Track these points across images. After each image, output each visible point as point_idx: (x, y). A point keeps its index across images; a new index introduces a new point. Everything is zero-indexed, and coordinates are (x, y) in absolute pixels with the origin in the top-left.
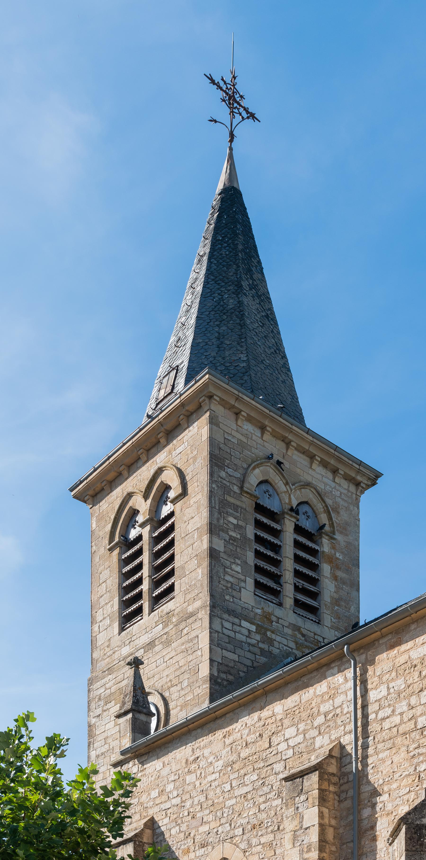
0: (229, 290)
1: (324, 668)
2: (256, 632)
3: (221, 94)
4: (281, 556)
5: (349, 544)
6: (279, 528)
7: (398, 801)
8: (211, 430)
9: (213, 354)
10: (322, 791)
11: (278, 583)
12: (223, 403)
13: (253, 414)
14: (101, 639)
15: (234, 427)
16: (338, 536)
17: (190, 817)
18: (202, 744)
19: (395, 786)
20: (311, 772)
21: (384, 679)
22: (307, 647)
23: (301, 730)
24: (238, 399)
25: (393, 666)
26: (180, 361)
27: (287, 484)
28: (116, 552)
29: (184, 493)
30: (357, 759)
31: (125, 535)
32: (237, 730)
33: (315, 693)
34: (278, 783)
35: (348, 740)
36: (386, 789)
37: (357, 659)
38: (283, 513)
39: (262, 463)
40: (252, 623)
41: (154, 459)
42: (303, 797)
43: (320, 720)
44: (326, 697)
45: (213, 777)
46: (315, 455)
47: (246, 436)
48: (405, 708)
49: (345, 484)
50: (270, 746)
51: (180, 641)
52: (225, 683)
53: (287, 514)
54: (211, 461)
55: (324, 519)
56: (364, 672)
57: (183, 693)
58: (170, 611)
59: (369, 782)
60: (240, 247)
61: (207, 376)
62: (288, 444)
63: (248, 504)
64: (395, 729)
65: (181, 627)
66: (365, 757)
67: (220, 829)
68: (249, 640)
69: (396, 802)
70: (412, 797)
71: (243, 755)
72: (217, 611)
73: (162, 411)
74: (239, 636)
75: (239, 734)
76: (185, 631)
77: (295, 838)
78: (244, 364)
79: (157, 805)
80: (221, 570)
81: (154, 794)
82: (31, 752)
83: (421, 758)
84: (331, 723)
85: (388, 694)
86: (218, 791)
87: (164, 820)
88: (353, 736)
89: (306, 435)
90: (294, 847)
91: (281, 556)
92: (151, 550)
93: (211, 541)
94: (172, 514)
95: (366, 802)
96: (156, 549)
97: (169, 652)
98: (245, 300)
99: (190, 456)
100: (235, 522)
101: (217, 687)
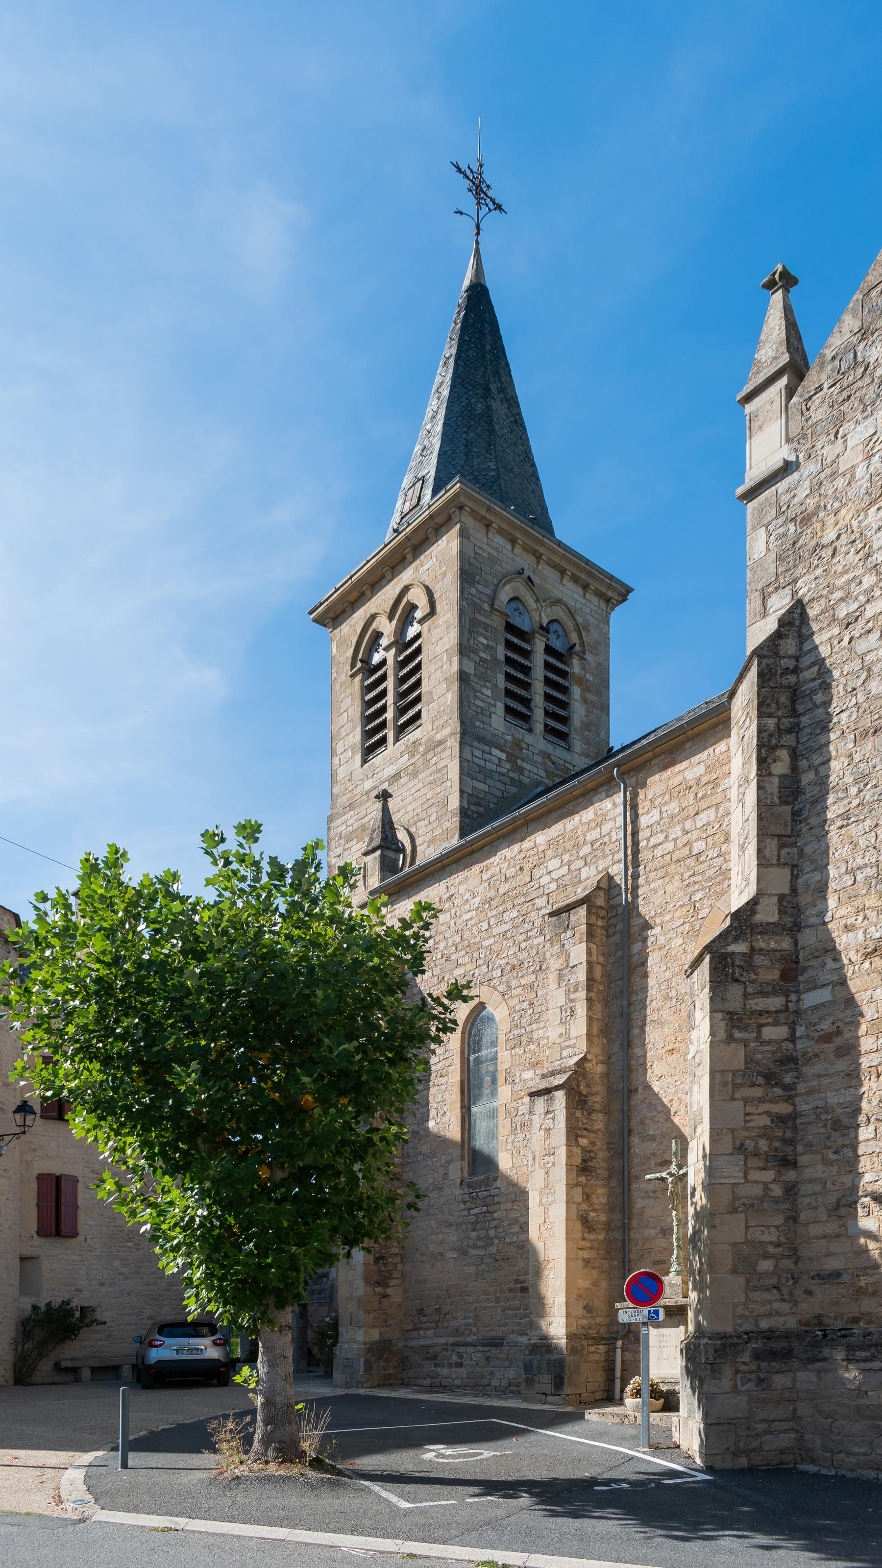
0: (476, 394)
1: (591, 794)
2: (506, 761)
3: (467, 184)
4: (531, 679)
5: (599, 664)
6: (529, 649)
7: (671, 934)
8: (461, 543)
9: (461, 462)
10: (589, 925)
11: (528, 707)
12: (474, 514)
13: (504, 526)
14: (342, 773)
15: (485, 540)
16: (588, 656)
17: (444, 959)
18: (457, 880)
19: (667, 917)
20: (579, 906)
21: (657, 803)
22: (557, 775)
23: (565, 861)
24: (489, 509)
25: (667, 788)
26: (427, 471)
27: (537, 601)
28: (359, 678)
29: (432, 612)
30: (627, 890)
31: (366, 661)
32: (495, 864)
33: (580, 820)
34: (541, 919)
35: (617, 870)
36: (658, 921)
37: (627, 782)
38: (534, 632)
39: (512, 579)
40: (502, 751)
41: (400, 577)
42: (569, 933)
43: (586, 849)
44: (593, 825)
45: (469, 915)
46: (566, 570)
47: (496, 549)
48: (679, 833)
49: (595, 600)
50: (531, 881)
51: (427, 772)
52: (475, 815)
53: (538, 633)
54: (461, 576)
55: (574, 638)
56: (635, 795)
57: (430, 827)
59: (639, 915)
60: (488, 348)
61: (458, 485)
62: (539, 557)
63: (498, 622)
64: (669, 856)
65: (429, 756)
66: (636, 888)
67: (477, 972)
68: (499, 769)
69: (669, 936)
70: (687, 929)
71: (501, 891)
72: (468, 739)
73: (409, 525)
74: (490, 766)
75: (498, 869)
76: (433, 761)
77: (560, 977)
78: (494, 473)
80: (472, 694)
82: (320, 884)
83: (697, 887)
84: (598, 853)
85: (661, 819)
86: (474, 930)
88: (622, 865)
89: (557, 548)
90: (559, 987)
91: (531, 679)
92: (396, 675)
93: (461, 663)
94: (418, 636)
95: (636, 936)
96: (401, 674)
97: (416, 784)
98: (494, 405)
99: (440, 572)
100: (485, 642)
101: (467, 820)
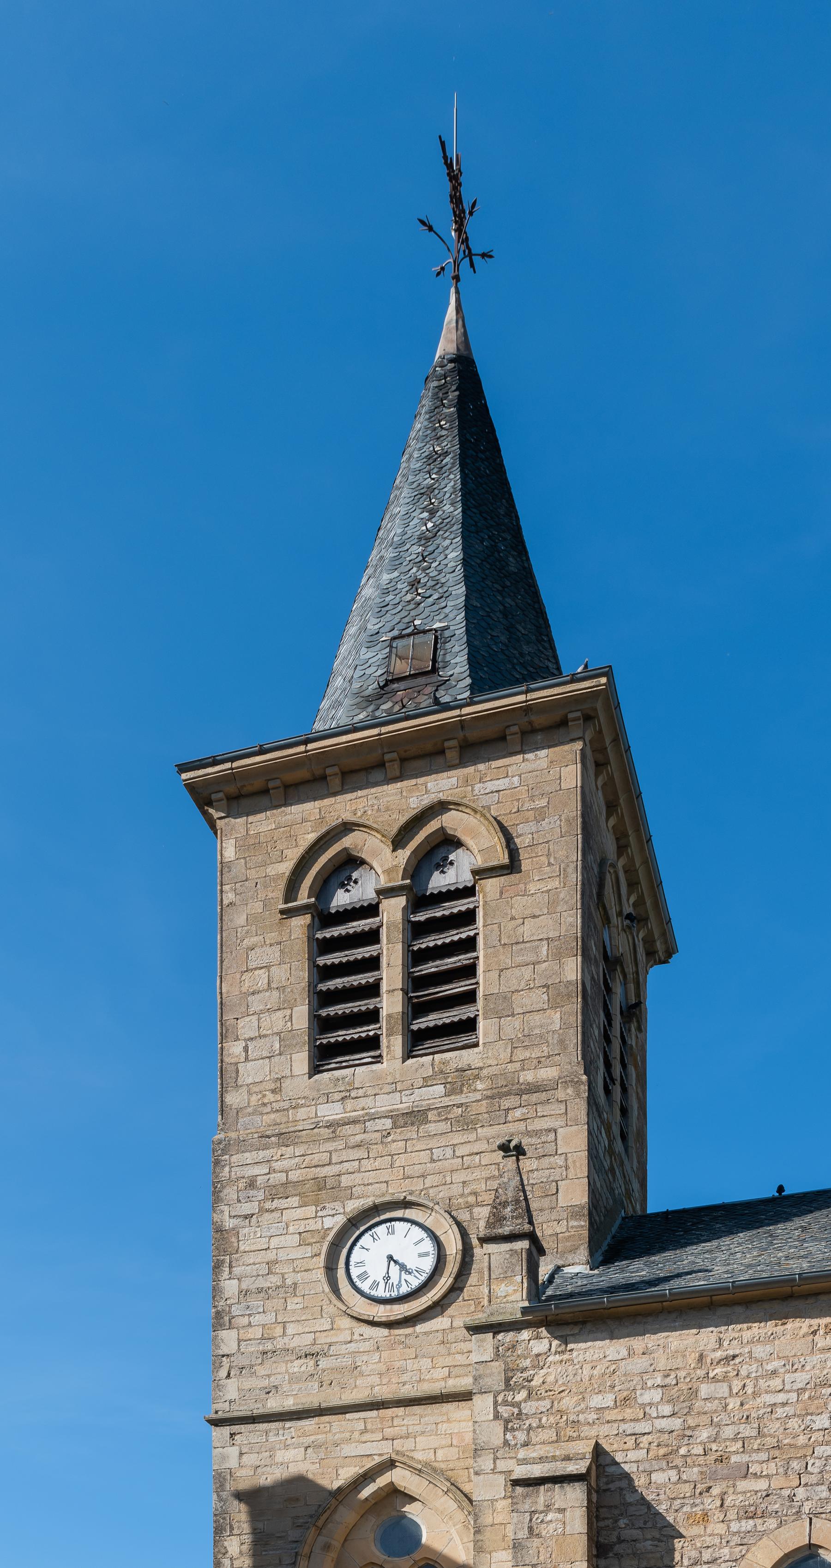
45: (781, 1398)
79: (608, 1422)
81: (608, 1400)
87: (629, 1453)
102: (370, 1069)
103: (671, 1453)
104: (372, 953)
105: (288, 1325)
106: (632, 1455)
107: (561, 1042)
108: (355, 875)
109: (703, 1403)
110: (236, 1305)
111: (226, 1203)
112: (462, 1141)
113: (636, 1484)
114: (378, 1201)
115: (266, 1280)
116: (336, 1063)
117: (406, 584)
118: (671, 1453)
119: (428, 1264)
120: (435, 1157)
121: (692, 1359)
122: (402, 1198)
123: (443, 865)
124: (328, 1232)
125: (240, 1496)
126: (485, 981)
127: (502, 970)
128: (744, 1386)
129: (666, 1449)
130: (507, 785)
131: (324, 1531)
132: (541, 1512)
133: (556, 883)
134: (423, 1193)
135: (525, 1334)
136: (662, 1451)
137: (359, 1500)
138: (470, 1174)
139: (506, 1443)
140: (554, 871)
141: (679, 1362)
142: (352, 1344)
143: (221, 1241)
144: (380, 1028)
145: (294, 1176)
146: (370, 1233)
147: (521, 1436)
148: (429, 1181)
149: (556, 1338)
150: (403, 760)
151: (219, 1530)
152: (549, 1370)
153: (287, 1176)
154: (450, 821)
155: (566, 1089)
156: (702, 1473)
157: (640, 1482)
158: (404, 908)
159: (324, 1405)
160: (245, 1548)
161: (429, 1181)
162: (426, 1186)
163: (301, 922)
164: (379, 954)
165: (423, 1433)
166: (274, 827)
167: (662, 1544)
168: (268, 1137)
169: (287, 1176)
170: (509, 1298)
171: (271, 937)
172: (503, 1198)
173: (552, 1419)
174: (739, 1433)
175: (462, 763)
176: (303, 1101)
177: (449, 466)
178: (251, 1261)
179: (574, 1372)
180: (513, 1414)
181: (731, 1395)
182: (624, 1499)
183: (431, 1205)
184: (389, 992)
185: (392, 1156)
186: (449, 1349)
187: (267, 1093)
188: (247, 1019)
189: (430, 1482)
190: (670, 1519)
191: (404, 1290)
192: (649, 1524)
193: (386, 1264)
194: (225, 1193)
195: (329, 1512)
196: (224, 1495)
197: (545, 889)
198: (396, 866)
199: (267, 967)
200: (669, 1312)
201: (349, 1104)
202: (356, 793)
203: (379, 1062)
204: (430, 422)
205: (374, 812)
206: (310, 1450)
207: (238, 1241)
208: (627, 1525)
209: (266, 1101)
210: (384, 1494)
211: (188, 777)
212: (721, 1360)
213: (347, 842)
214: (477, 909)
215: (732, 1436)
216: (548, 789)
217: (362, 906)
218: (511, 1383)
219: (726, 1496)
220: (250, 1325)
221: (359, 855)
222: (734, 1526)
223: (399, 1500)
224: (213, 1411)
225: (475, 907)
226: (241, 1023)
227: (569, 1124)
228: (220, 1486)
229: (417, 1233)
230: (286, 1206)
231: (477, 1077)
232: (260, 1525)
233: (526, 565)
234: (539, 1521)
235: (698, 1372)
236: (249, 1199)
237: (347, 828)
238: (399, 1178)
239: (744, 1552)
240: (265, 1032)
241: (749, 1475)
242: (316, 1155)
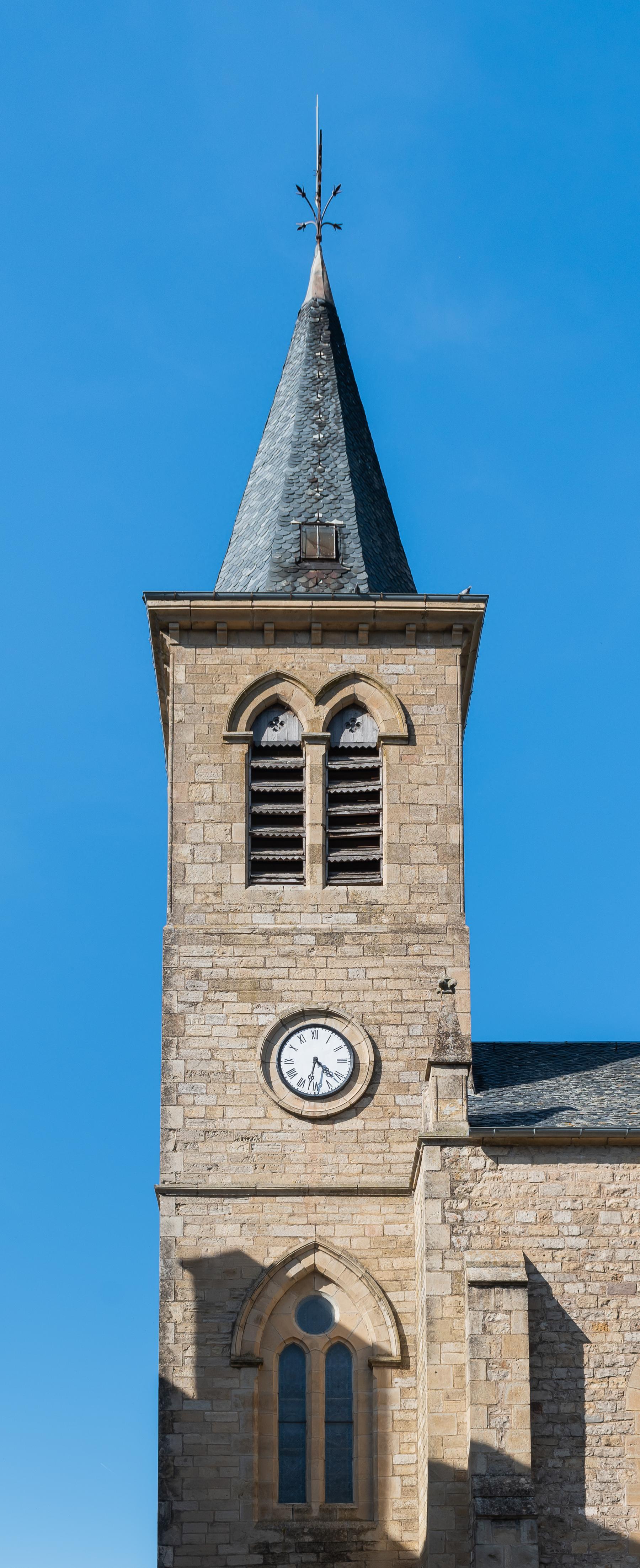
58: (374, 902)
79: (531, 1236)
81: (529, 1216)
102: (296, 889)
103: (578, 1268)
104: (297, 788)
105: (227, 1108)
106: (550, 1267)
107: (448, 894)
108: (281, 718)
109: (602, 1227)
110: (183, 1084)
111: (174, 988)
112: (372, 966)
113: (554, 1292)
114: (306, 1007)
115: (209, 1065)
116: (267, 878)
117: (306, 480)
118: (578, 1268)
119: (345, 1070)
120: (350, 976)
121: (593, 1189)
122: (326, 1008)
123: (352, 725)
124: (262, 1028)
125: (185, 1264)
126: (388, 831)
127: (401, 824)
128: (632, 1216)
129: (575, 1264)
130: (404, 671)
131: (257, 1305)
132: (492, 1312)
133: (441, 760)
134: (341, 1006)
135: (466, 1151)
136: (572, 1266)
137: (288, 1277)
138: (378, 996)
139: (452, 1245)
140: (441, 750)
141: (583, 1190)
142: (282, 1133)
143: (170, 1023)
144: (303, 855)
145: (234, 973)
146: (298, 1034)
147: (464, 1241)
148: (346, 996)
149: (490, 1157)
150: (324, 631)
151: (164, 1295)
152: (485, 1185)
153: (228, 972)
154: (360, 689)
155: (453, 935)
156: (602, 1288)
157: (556, 1291)
158: (324, 756)
159: (259, 1187)
160: (189, 1314)
161: (346, 996)
162: (343, 1000)
163: (241, 749)
164: (302, 790)
165: (341, 1221)
166: (217, 662)
167: (574, 1347)
168: (212, 934)
169: (228, 972)
170: (452, 1117)
171: (215, 757)
172: (445, 1029)
173: (488, 1229)
174: (629, 1256)
175: (369, 645)
176: (240, 908)
177: (330, 391)
178: (196, 1045)
179: (504, 1189)
180: (457, 1220)
181: (623, 1223)
182: (544, 1305)
183: (349, 1018)
184: (312, 825)
185: (316, 969)
186: (363, 1147)
187: (210, 895)
188: (194, 826)
189: (347, 1267)
190: (580, 1325)
191: (324, 1090)
192: (564, 1329)
193: (312, 1064)
194: (174, 979)
195: (261, 1287)
196: (170, 1261)
197: (434, 763)
198: (318, 718)
199: (212, 783)
200: (576, 1146)
201: (280, 917)
202: (285, 649)
203: (302, 884)
204: (312, 350)
205: (300, 669)
206: (245, 1227)
207: (185, 1025)
208: (547, 1328)
209: (209, 901)
210: (305, 1274)
211: (153, 605)
212: (614, 1192)
213: (279, 689)
214: (380, 769)
215: (624, 1259)
216: (436, 681)
217: (287, 746)
218: (456, 1192)
219: (620, 1310)
220: (194, 1104)
221: (287, 702)
222: (628, 1337)
223: (317, 1281)
224: (161, 1181)
225: (379, 767)
226: (189, 828)
227: (456, 965)
228: (166, 1253)
229: (337, 1041)
230: (226, 999)
231: (382, 912)
232: (201, 1294)
233: (377, 486)
234: (491, 1320)
235: (598, 1200)
236: (195, 988)
237: (278, 677)
238: (321, 989)
239: (635, 1359)
240: (208, 840)
241: (637, 1293)
242: (252, 958)
